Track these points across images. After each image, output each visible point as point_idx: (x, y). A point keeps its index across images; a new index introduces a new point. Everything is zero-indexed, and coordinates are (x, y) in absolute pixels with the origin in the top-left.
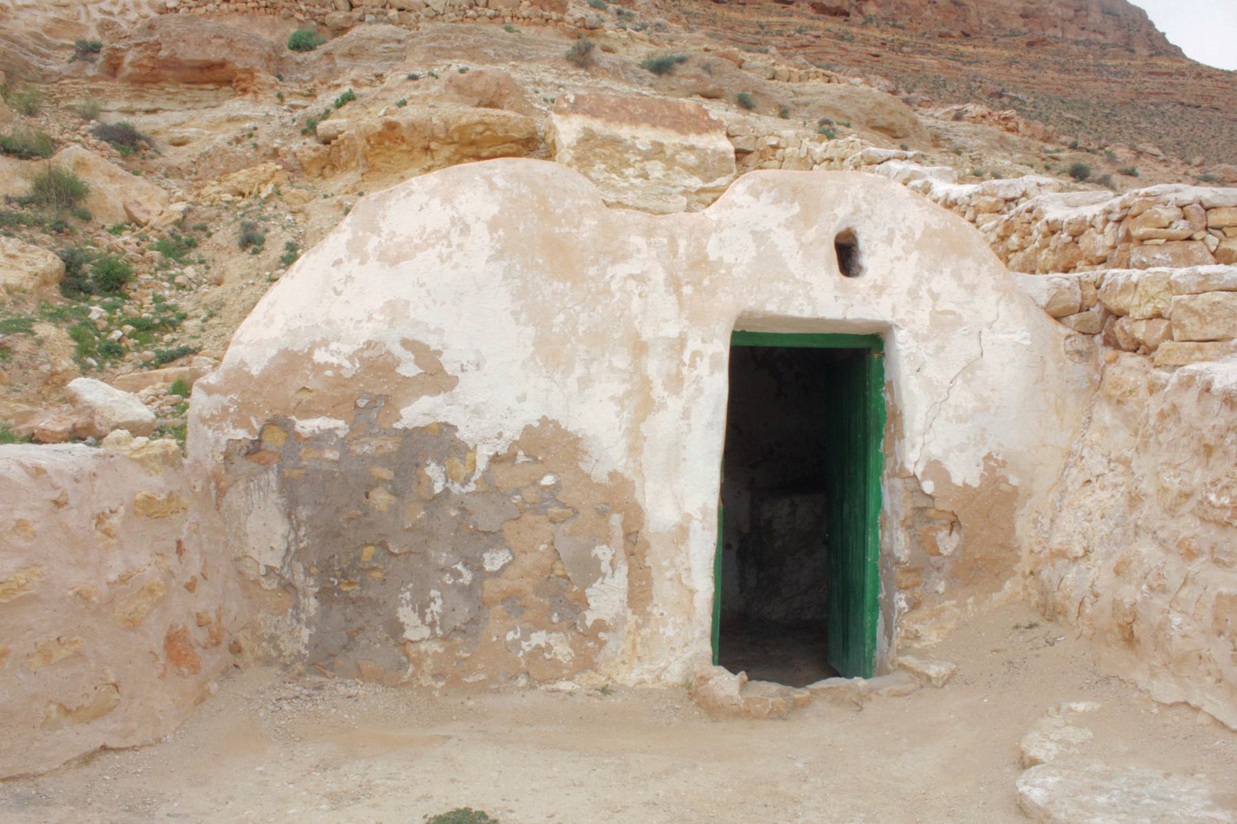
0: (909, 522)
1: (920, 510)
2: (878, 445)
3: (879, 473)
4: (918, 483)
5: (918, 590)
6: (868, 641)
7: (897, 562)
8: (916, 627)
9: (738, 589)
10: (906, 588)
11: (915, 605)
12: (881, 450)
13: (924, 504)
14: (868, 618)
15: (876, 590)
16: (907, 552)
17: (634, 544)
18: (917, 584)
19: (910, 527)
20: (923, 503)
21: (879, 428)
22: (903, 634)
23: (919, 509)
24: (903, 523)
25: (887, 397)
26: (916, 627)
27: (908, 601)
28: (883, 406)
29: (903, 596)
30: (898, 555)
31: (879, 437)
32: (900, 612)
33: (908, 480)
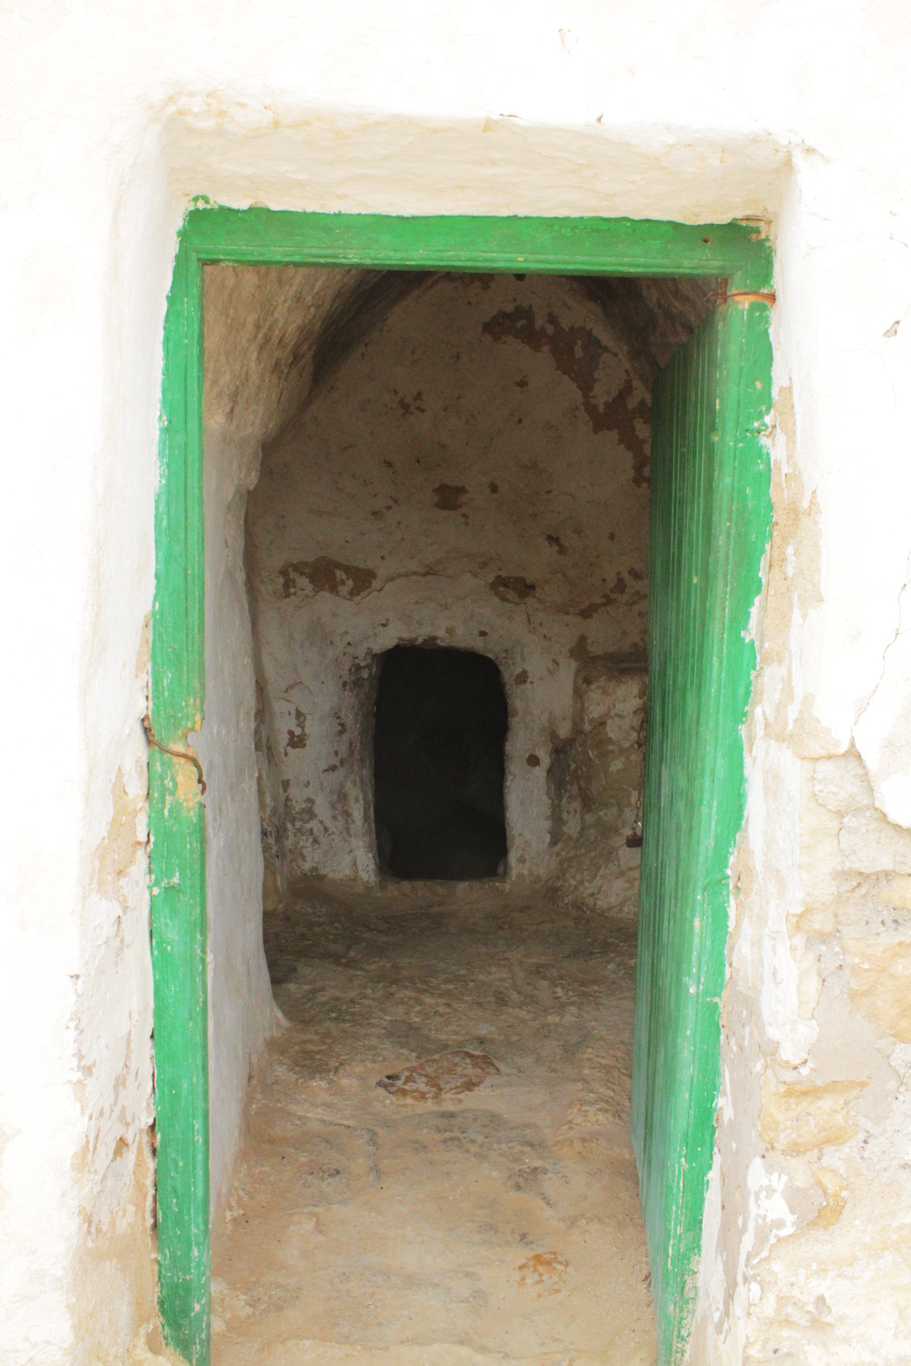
0: (820, 922)
1: (864, 881)
2: (740, 618)
3: (741, 716)
4: (867, 782)
5: (834, 1158)
6: (677, 1229)
7: (769, 1051)
8: (819, 1286)
9: (548, 838)
10: (795, 1150)
11: (821, 1212)
12: (750, 635)
13: (886, 863)
14: (679, 1163)
15: (709, 1086)
16: (807, 1032)
17: (295, 960)
18: (833, 1138)
19: (824, 938)
20: (876, 855)
21: (746, 560)
22: (769, 1307)
23: (863, 877)
24: (799, 923)
25: (776, 448)
26: (819, 1286)
27: (794, 1197)
28: (765, 478)
29: (779, 1182)
30: (773, 1033)
31: (748, 587)
32: (762, 1237)
33: (825, 769)
